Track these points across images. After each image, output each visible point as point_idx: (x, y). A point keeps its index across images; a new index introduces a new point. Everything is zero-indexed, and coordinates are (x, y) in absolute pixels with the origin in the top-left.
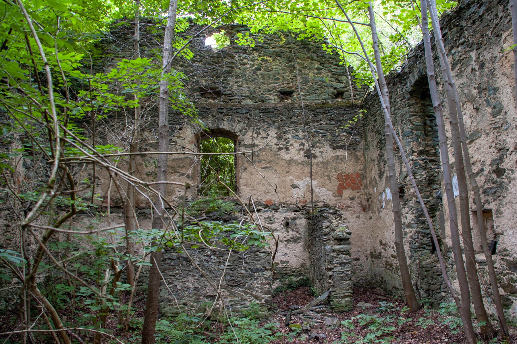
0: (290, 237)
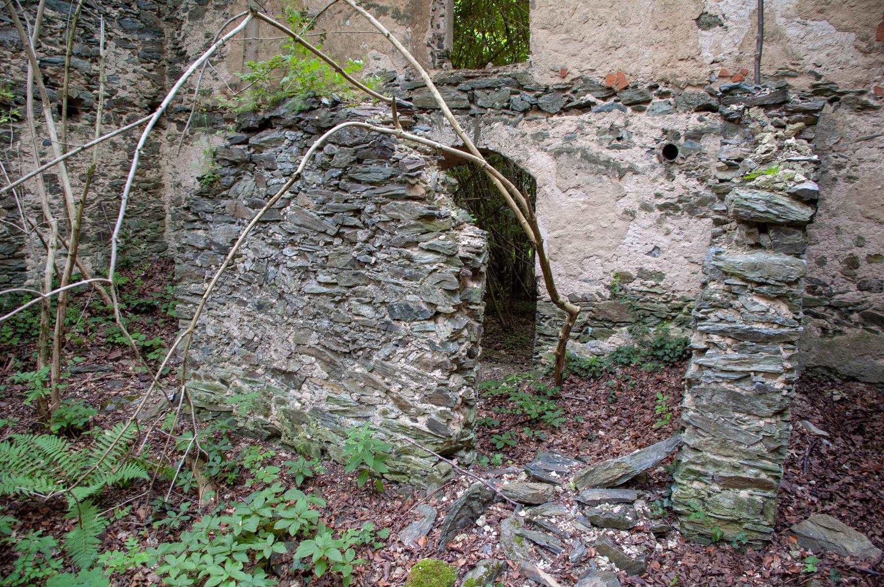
0: (676, 194)
